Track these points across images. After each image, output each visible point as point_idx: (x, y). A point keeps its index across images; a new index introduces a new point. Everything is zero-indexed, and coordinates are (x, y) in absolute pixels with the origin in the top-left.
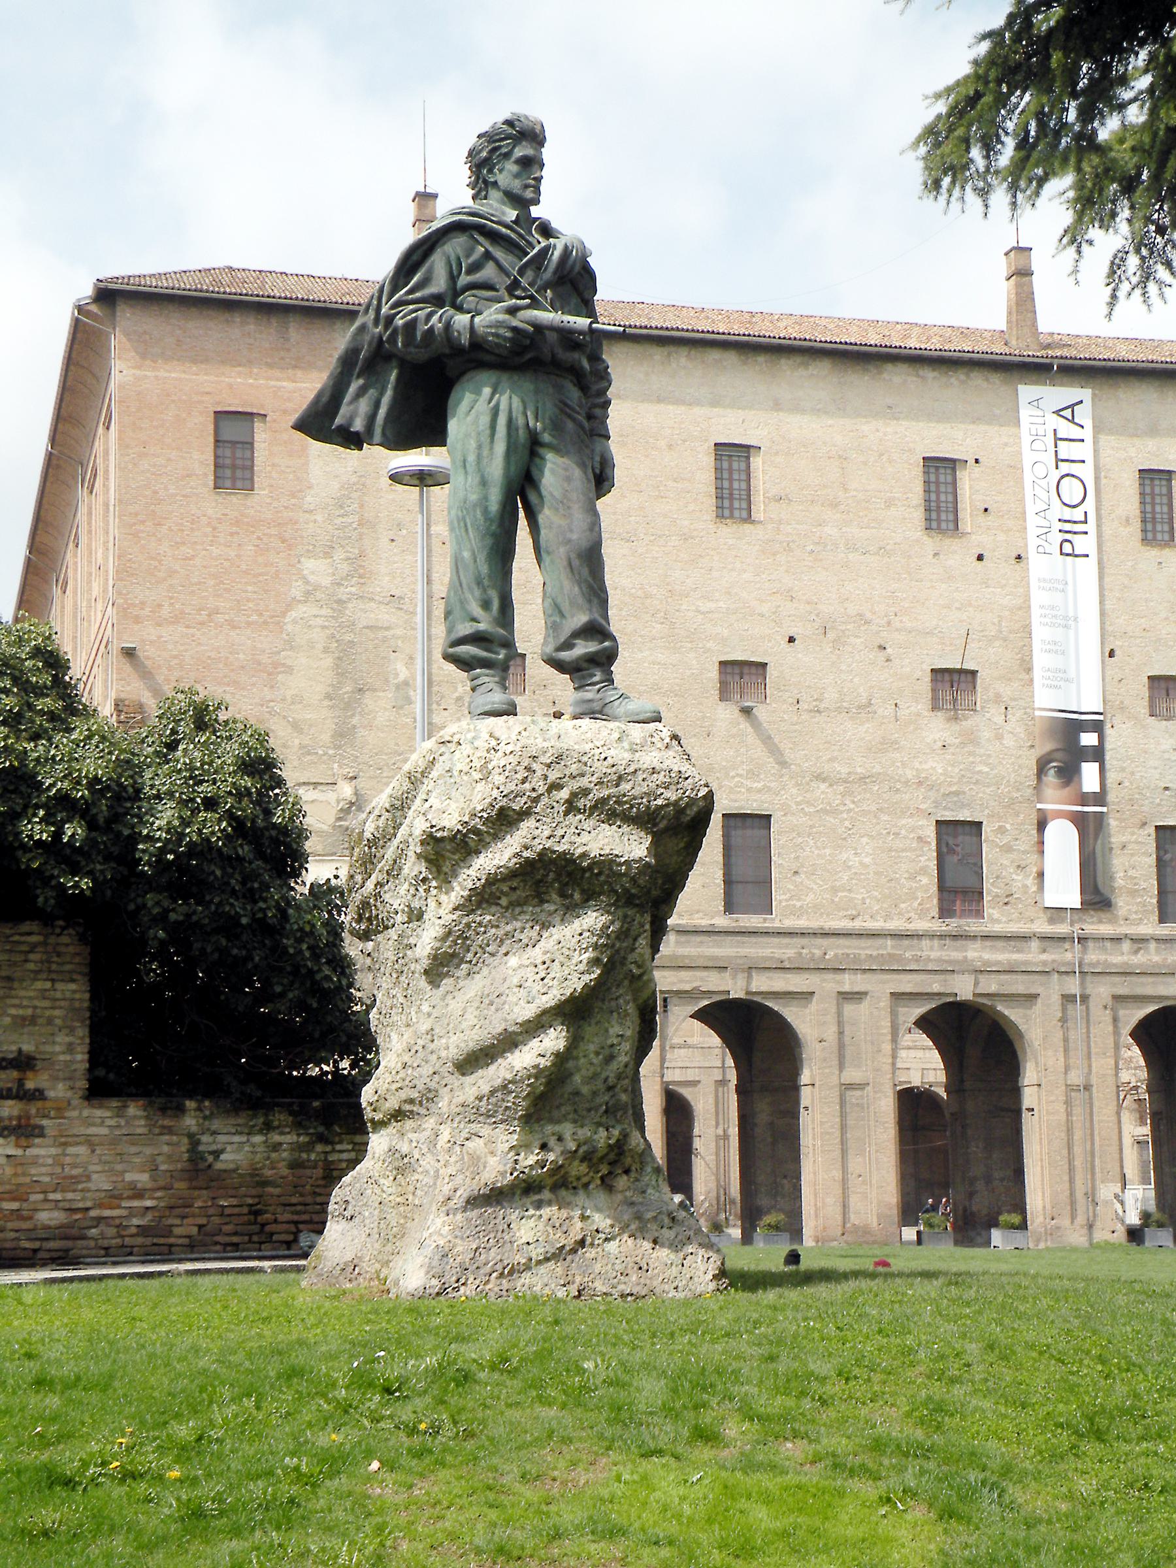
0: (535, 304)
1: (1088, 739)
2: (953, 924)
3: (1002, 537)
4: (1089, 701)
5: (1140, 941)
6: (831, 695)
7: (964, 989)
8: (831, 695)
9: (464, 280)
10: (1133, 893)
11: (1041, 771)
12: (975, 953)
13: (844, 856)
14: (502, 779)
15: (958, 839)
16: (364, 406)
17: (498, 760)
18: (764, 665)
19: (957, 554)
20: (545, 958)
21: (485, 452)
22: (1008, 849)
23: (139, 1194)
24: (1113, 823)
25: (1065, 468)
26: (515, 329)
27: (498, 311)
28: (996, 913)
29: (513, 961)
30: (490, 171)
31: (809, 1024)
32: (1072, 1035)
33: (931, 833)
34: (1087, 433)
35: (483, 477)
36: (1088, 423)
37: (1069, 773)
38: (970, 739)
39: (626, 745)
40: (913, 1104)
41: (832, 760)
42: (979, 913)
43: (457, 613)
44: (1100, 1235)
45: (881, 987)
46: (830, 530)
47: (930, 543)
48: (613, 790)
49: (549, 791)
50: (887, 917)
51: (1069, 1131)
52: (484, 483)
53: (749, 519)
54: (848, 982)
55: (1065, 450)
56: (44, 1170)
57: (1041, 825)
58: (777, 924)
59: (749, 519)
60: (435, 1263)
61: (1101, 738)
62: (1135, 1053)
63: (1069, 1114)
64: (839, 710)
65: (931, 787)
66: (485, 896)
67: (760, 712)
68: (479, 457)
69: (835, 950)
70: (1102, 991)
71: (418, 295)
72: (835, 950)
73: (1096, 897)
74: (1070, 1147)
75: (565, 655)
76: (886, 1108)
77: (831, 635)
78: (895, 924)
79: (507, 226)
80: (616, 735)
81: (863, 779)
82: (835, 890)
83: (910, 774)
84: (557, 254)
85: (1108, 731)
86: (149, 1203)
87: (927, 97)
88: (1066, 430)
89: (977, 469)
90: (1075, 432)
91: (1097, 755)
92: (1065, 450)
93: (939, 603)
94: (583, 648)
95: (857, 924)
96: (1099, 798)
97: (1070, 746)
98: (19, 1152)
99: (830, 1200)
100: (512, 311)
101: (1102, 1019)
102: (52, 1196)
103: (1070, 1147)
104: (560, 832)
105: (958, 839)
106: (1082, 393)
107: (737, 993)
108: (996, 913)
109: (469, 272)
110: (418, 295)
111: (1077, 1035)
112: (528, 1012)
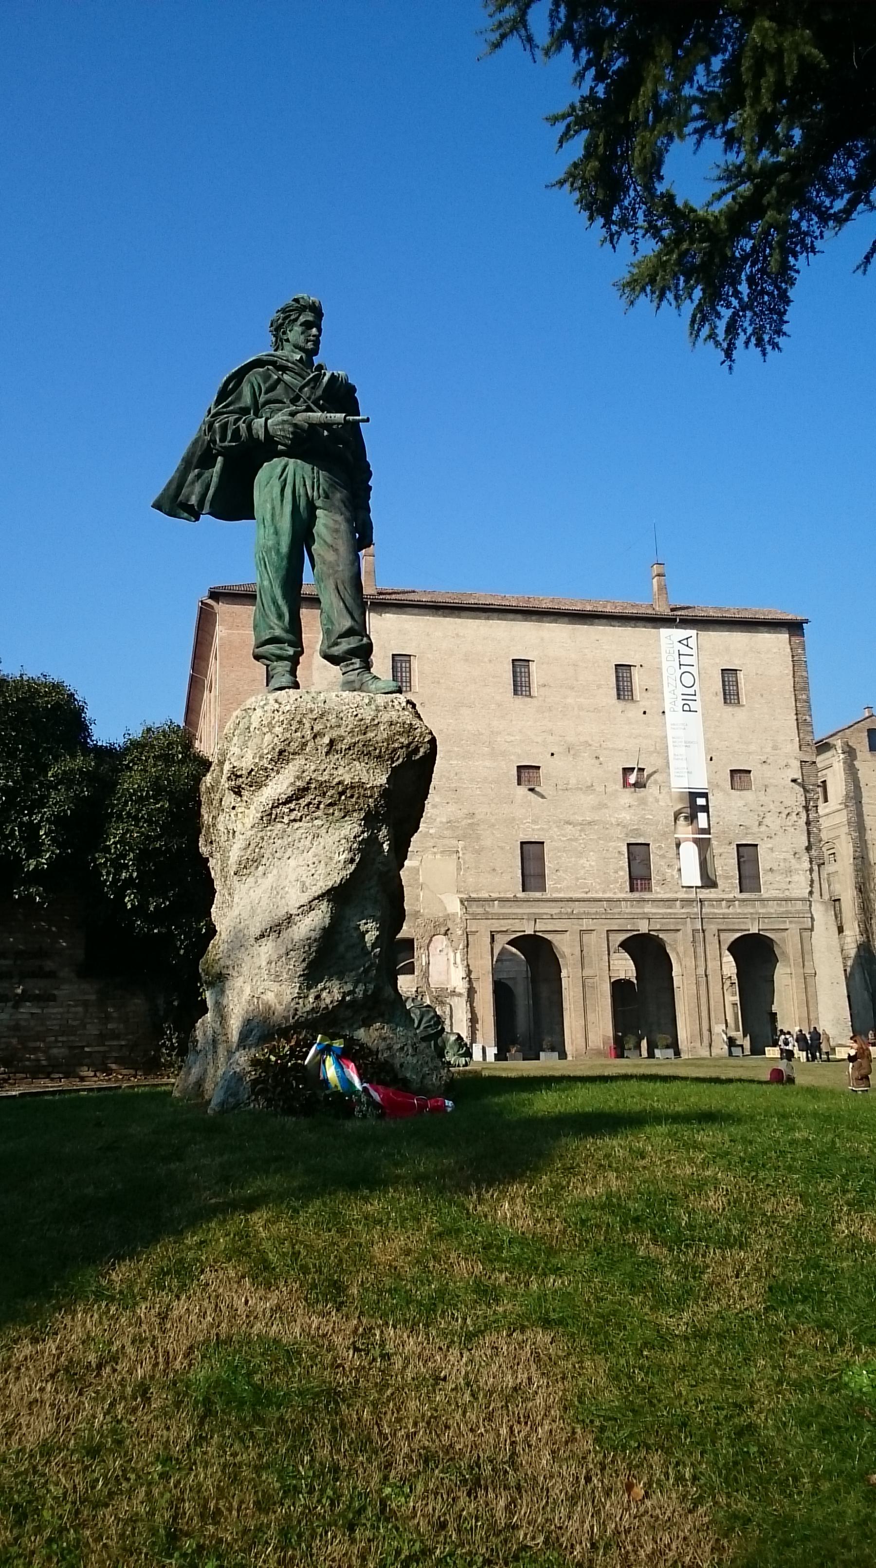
0: (309, 409)
1: (701, 801)
2: (636, 895)
3: (655, 702)
4: (700, 783)
5: (731, 902)
6: (573, 781)
7: (643, 927)
8: (573, 781)
9: (262, 399)
10: (727, 878)
11: (676, 819)
12: (648, 909)
13: (582, 861)
14: (281, 730)
15: (638, 857)
16: (198, 488)
17: (279, 717)
18: (538, 768)
19: (633, 711)
20: (315, 859)
21: (278, 511)
22: (663, 857)
23: (117, 1037)
24: (714, 842)
25: (684, 669)
26: (295, 426)
27: (284, 414)
28: (658, 889)
29: (292, 862)
30: (284, 333)
31: (565, 947)
32: (698, 950)
33: (625, 849)
34: (694, 652)
35: (276, 528)
36: (695, 647)
37: (692, 818)
38: (643, 802)
39: (373, 707)
40: (619, 988)
41: (574, 814)
42: (650, 890)
43: (262, 625)
44: (716, 1051)
45: (602, 927)
46: (569, 700)
47: (621, 705)
48: (361, 737)
49: (315, 737)
50: (604, 892)
51: (698, 999)
52: (276, 533)
53: (530, 696)
54: (586, 924)
55: (684, 660)
56: (55, 1022)
57: (678, 845)
58: (549, 896)
59: (530, 696)
60: (233, 1084)
61: (707, 801)
62: (729, 959)
63: (698, 990)
64: (577, 789)
65: (624, 827)
66: (269, 817)
67: (538, 789)
68: (273, 515)
69: (578, 908)
70: (712, 928)
71: (231, 408)
72: (578, 908)
73: (708, 882)
74: (699, 1006)
75: (337, 651)
76: (606, 988)
77: (572, 752)
78: (607, 895)
79: (293, 363)
80: (367, 701)
81: (590, 823)
82: (577, 879)
83: (613, 820)
84: (326, 379)
85: (710, 796)
86: (123, 1043)
87: (555, 119)
88: (684, 650)
89: (642, 670)
90: (689, 651)
91: (705, 809)
92: (684, 660)
93: (623, 735)
94: (345, 645)
95: (589, 895)
96: (707, 831)
97: (694, 805)
98: (39, 1011)
99: (578, 1036)
100: (293, 414)
101: (712, 941)
102: (60, 1039)
103: (699, 1006)
104: (323, 767)
105: (638, 857)
106: (692, 632)
107: (530, 931)
108: (658, 889)
109: (266, 393)
110: (231, 408)
111: (700, 950)
112: (304, 899)
